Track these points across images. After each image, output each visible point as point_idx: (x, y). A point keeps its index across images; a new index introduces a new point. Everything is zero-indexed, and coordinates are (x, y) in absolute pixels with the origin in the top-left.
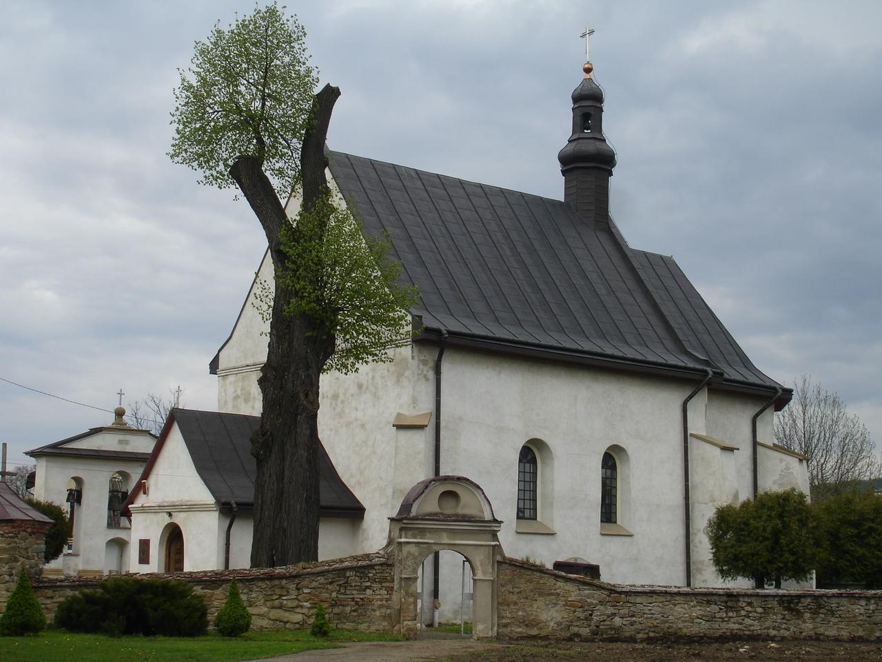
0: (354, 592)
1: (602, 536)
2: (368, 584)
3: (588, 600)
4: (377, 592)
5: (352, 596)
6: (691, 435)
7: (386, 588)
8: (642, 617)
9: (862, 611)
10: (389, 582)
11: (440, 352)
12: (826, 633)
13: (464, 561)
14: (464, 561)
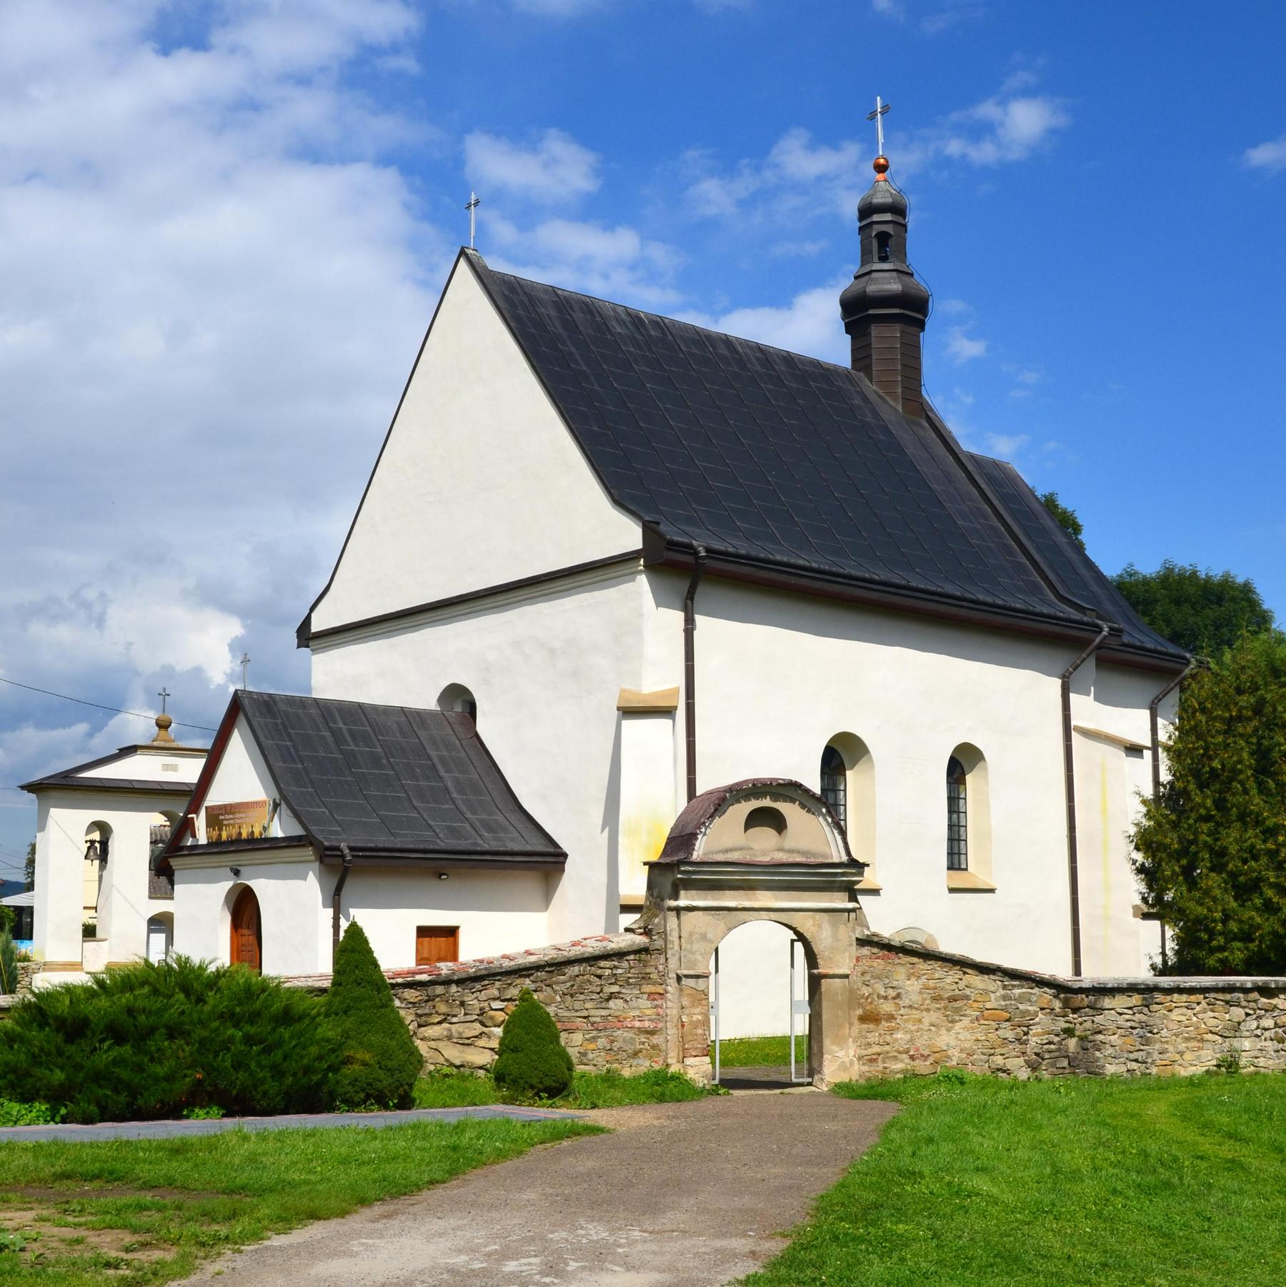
0: (588, 1005)
2: (615, 989)
3: (1021, 1007)
5: (585, 1013)
6: (1087, 733)
7: (651, 996)
10: (654, 984)
13: (793, 941)
14: (793, 941)
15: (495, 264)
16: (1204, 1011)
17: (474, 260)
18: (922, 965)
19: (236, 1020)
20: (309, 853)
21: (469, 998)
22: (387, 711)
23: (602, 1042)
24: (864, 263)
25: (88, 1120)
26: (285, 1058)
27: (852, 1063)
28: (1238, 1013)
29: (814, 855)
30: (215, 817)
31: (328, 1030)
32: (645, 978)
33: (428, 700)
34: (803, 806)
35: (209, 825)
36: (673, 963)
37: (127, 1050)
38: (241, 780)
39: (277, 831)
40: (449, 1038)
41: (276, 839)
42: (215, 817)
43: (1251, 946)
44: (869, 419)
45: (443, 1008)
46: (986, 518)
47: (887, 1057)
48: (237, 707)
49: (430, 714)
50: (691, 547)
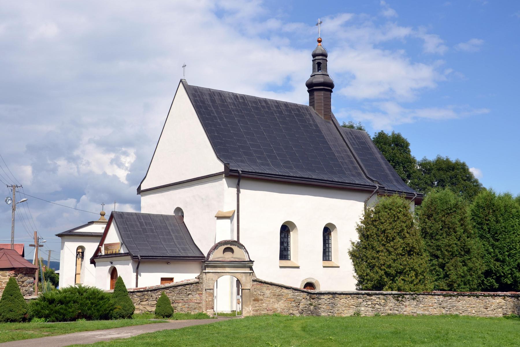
2: (190, 292)
4: (195, 296)
9: (436, 301)
12: (418, 313)
15: (190, 83)
16: (351, 300)
17: (184, 83)
18: (270, 287)
19: (89, 298)
20: (129, 257)
21: (153, 295)
22: (157, 216)
23: (186, 306)
24: (313, 72)
25: (53, 321)
26: (101, 307)
27: (250, 311)
28: (360, 300)
29: (241, 259)
30: (106, 248)
31: (112, 301)
32: (198, 290)
33: (171, 213)
34: (238, 247)
35: (105, 249)
36: (204, 286)
37: (63, 306)
38: (113, 237)
39: (122, 251)
40: (148, 305)
41: (122, 254)
42: (107, 247)
43: (373, 283)
44: (311, 122)
45: (147, 297)
46: (346, 152)
47: (261, 310)
48: (112, 217)
49: (171, 216)
50: (237, 171)
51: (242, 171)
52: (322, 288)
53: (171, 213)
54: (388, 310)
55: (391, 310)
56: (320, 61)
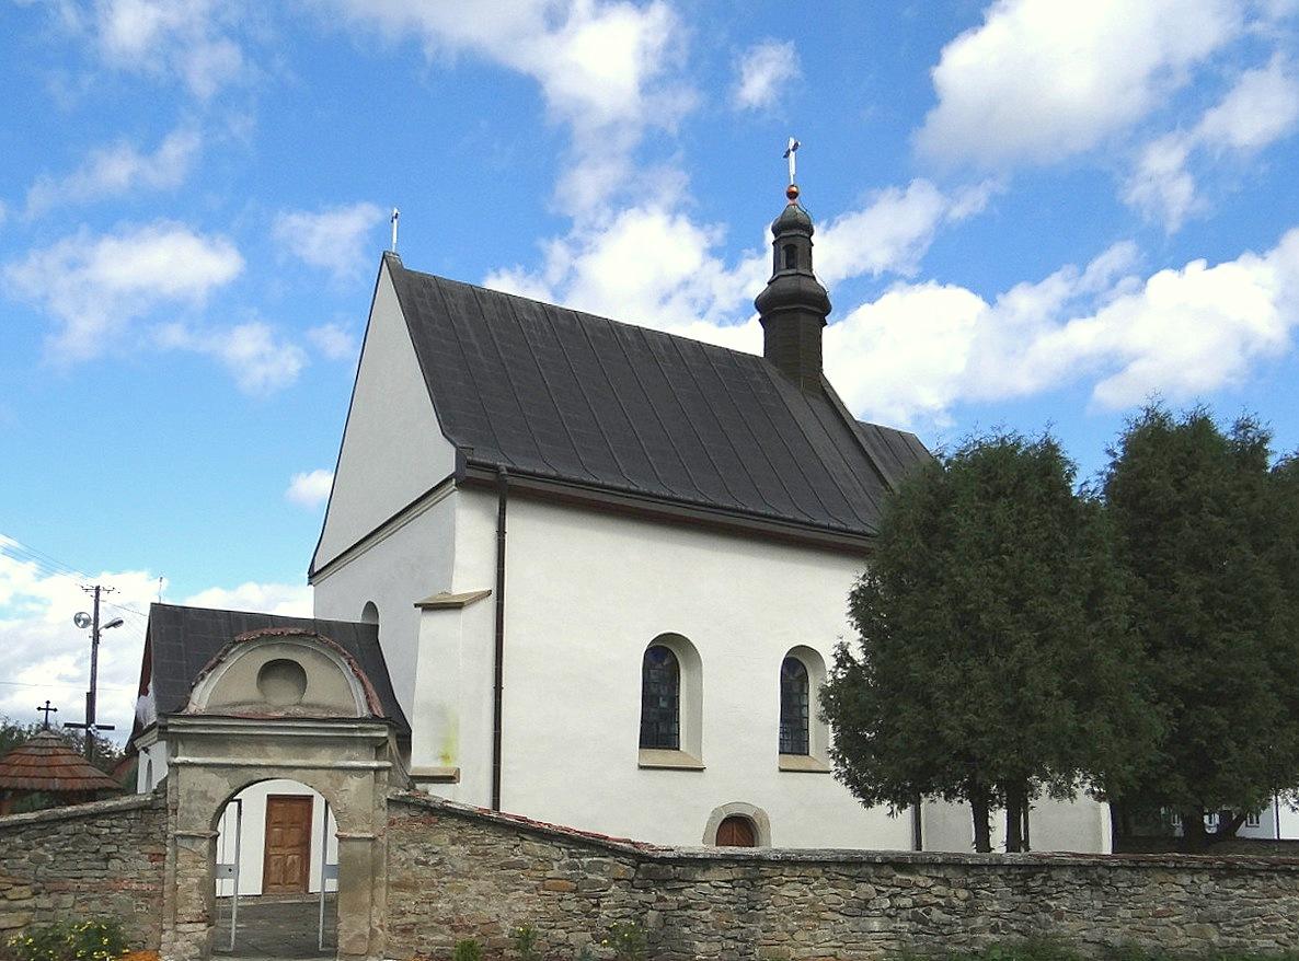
1: (641, 771)
2: (113, 848)
3: (590, 876)
8: (706, 909)
9: (1184, 896)
11: (500, 504)
15: (415, 264)
16: (823, 887)
28: (867, 889)
29: (335, 710)
32: (146, 838)
51: (508, 469)
52: (781, 837)
53: (357, 618)
54: (981, 930)
55: (994, 930)
56: (793, 241)
